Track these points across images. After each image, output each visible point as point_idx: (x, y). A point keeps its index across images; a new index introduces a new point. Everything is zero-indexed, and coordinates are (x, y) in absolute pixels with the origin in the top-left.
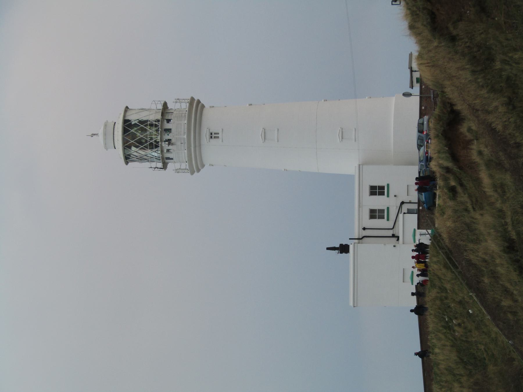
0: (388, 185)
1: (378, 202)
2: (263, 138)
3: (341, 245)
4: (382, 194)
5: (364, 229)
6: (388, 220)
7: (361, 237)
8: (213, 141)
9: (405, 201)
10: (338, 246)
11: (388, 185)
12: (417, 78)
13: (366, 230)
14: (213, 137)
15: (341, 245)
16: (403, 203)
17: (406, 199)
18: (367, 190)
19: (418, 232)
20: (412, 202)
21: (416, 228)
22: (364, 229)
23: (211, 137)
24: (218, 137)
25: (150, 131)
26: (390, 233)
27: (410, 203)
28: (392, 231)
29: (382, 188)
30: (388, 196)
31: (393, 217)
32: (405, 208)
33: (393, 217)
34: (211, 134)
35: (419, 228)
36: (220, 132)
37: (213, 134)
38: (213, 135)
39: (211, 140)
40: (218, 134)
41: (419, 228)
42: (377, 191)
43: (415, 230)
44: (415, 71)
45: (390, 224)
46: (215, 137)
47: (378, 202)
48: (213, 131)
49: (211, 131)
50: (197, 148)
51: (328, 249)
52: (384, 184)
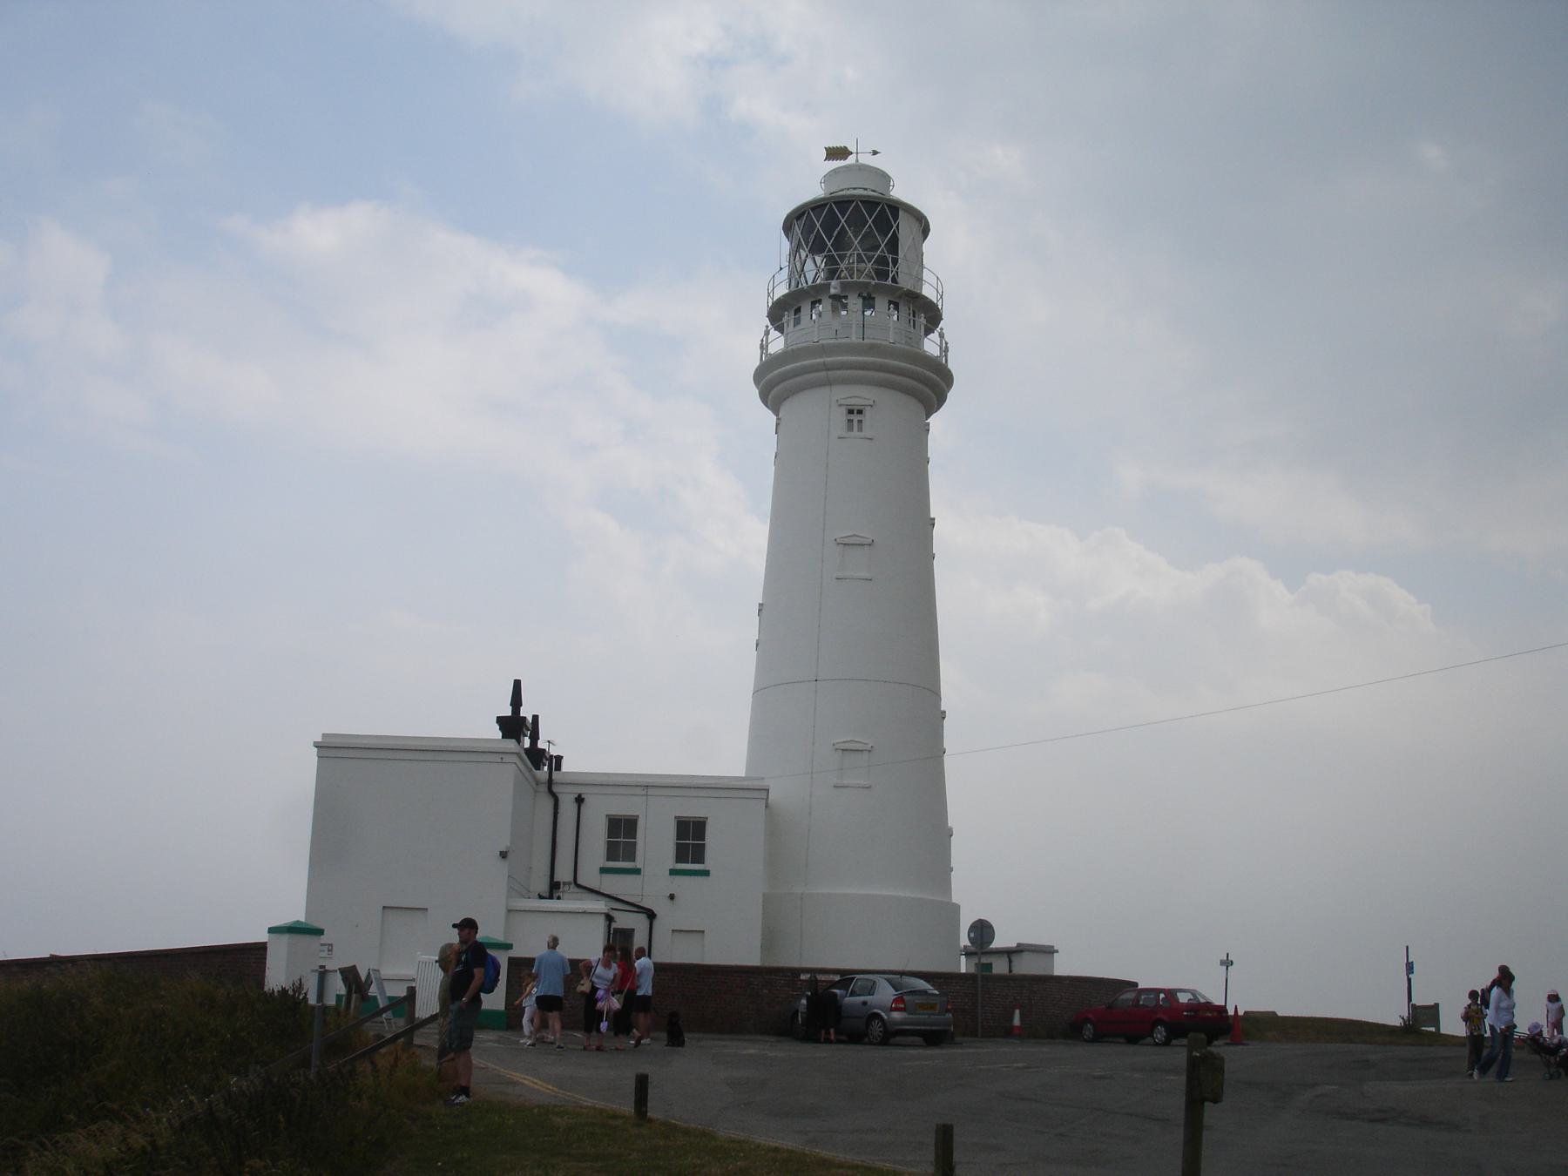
1: (656, 843)
2: (846, 541)
5: (580, 800)
6: (604, 870)
7: (555, 789)
8: (840, 416)
9: (656, 923)
11: (706, 873)
13: (575, 806)
14: (851, 417)
16: (651, 915)
18: (692, 810)
22: (580, 800)
23: (851, 412)
24: (850, 429)
26: (564, 874)
28: (570, 878)
29: (699, 856)
30: (673, 872)
31: (612, 884)
33: (612, 884)
34: (860, 412)
36: (866, 433)
37: (860, 417)
38: (855, 418)
39: (844, 410)
40: (860, 429)
42: (691, 839)
45: (589, 876)
46: (850, 421)
47: (656, 843)
49: (867, 411)
50: (823, 374)
51: (517, 684)
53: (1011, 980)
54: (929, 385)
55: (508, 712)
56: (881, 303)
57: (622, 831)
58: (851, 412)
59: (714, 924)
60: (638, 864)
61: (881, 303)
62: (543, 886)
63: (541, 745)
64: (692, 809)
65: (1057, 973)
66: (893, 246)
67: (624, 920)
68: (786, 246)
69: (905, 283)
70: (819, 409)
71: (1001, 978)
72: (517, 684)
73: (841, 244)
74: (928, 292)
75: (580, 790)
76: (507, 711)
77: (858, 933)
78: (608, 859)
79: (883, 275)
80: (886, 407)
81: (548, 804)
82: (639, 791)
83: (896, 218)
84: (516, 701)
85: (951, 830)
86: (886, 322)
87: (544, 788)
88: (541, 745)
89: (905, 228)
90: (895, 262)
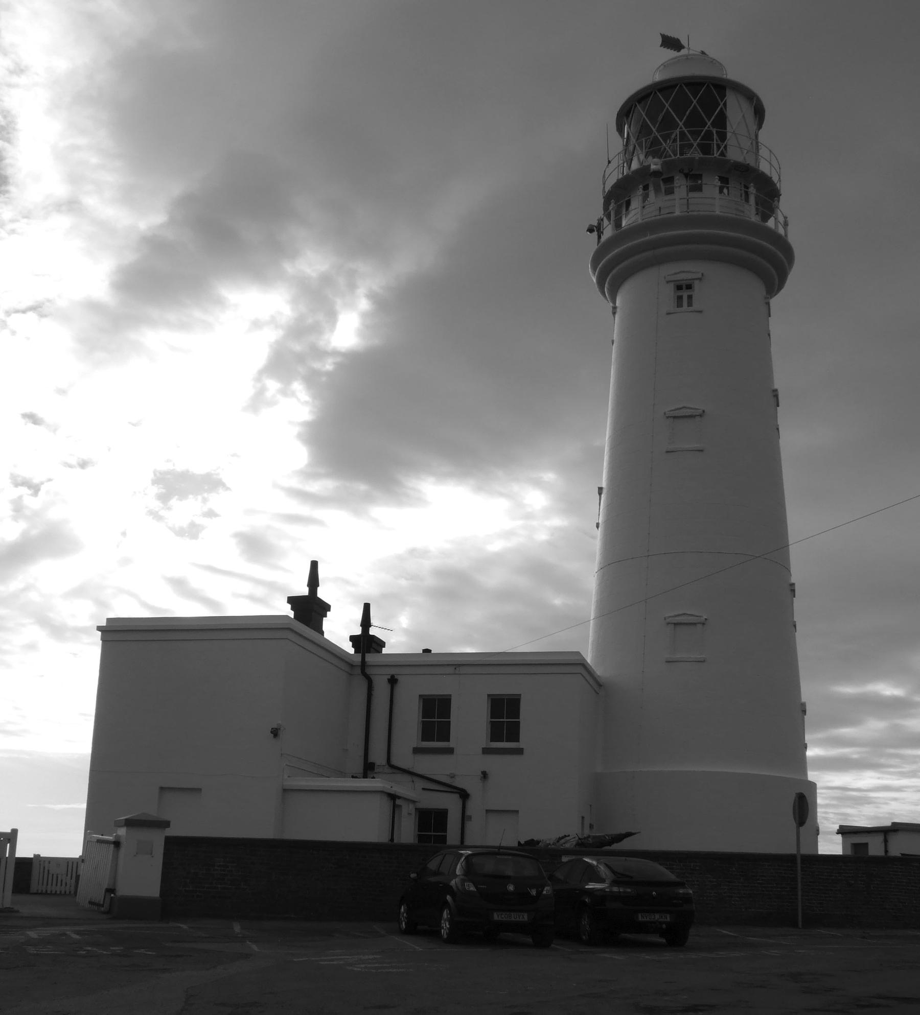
0: (520, 751)
1: (470, 722)
2: (676, 413)
3: (325, 608)
4: (496, 735)
5: (393, 681)
6: (417, 751)
7: (369, 671)
8: (669, 291)
10: (322, 593)
11: (450, 751)
12: (866, 845)
13: (387, 687)
14: (680, 293)
15: (325, 608)
16: (464, 795)
17: (475, 807)
19: (157, 839)
20: (469, 825)
21: (171, 832)
22: (393, 681)
23: (679, 288)
25: (695, 145)
26: (378, 756)
27: (464, 818)
28: (384, 762)
30: (486, 751)
31: (429, 765)
32: (451, 803)
33: (429, 765)
34: (689, 287)
35: (171, 842)
36: (696, 306)
37: (689, 292)
38: (685, 294)
39: (672, 285)
40: (690, 304)
41: (171, 842)
42: (505, 716)
43: (166, 824)
44: (886, 841)
45: (403, 756)
46: (680, 298)
47: (470, 722)
48: (696, 292)
49: (696, 285)
51: (314, 565)
52: (524, 741)
53: (886, 861)
54: (770, 263)
55: (304, 591)
56: (711, 185)
57: (436, 715)
58: (679, 288)
59: (528, 802)
60: (451, 744)
61: (711, 185)
62: (359, 767)
63: (372, 631)
64: (504, 687)
65: (820, 853)
66: (721, 121)
67: (451, 803)
68: (617, 144)
69: (734, 155)
70: (647, 288)
71: (876, 860)
72: (314, 565)
73: (667, 124)
74: (764, 167)
75: (393, 671)
76: (358, 631)
77: (688, 814)
78: (423, 740)
79: (706, 149)
80: (721, 286)
81: (361, 686)
82: (450, 670)
83: (723, 96)
84: (314, 581)
85: (803, 705)
86: (713, 200)
87: (359, 671)
88: (372, 631)
89: (736, 111)
90: (723, 137)
